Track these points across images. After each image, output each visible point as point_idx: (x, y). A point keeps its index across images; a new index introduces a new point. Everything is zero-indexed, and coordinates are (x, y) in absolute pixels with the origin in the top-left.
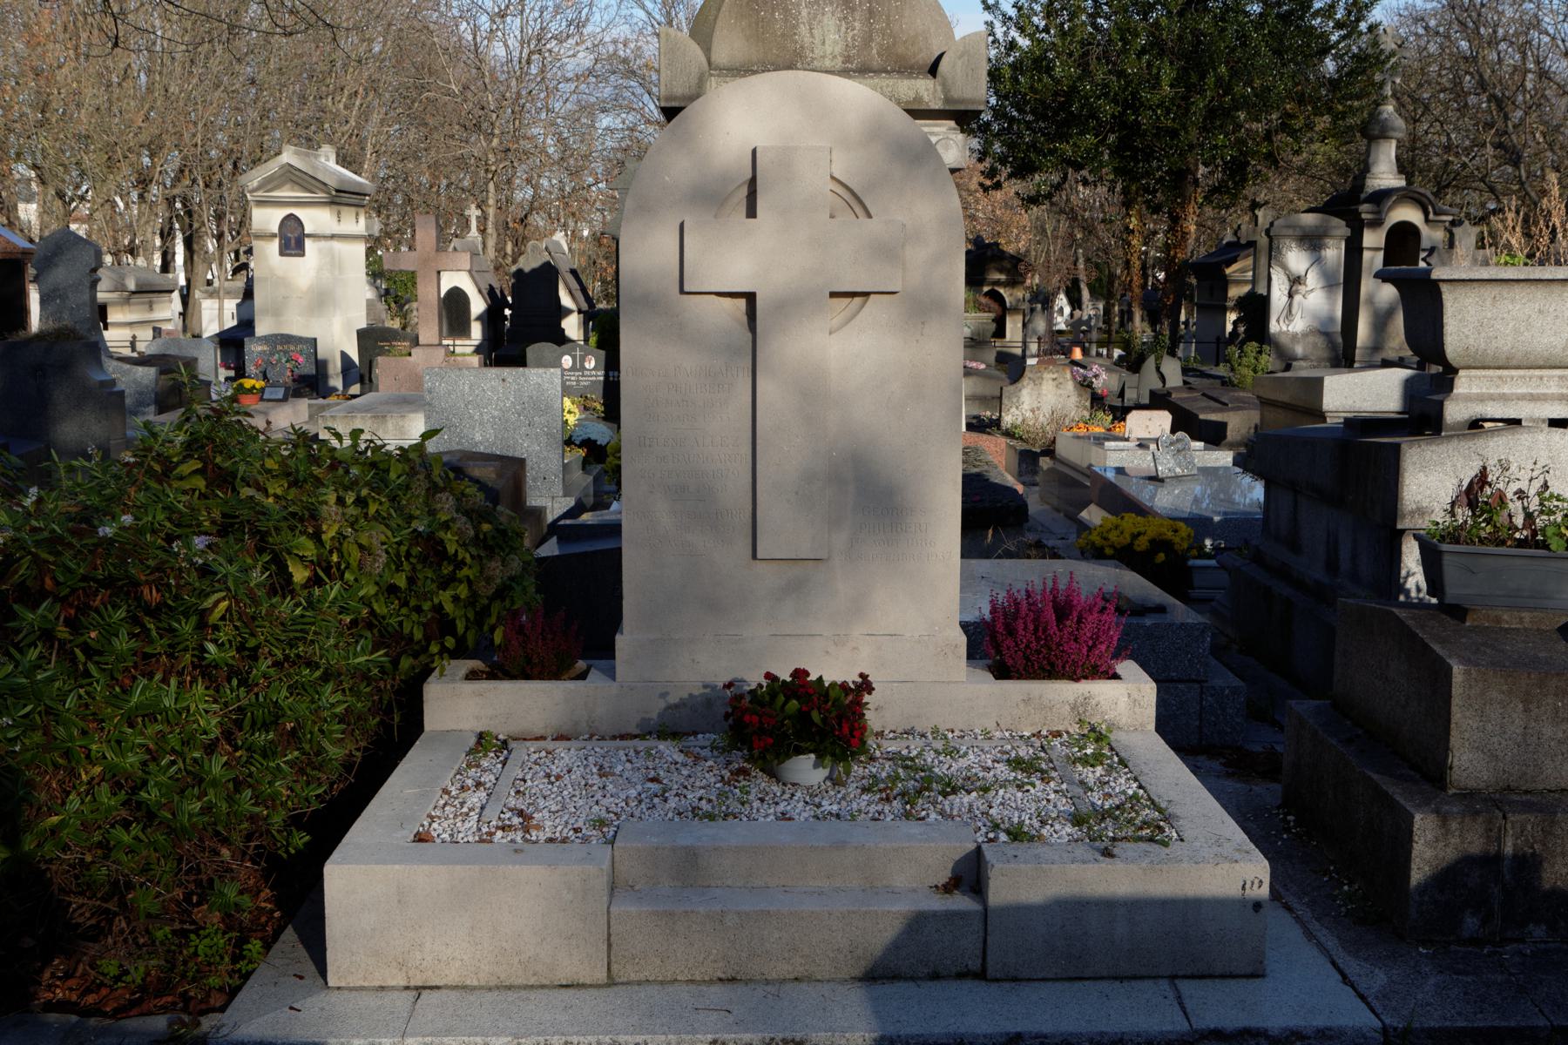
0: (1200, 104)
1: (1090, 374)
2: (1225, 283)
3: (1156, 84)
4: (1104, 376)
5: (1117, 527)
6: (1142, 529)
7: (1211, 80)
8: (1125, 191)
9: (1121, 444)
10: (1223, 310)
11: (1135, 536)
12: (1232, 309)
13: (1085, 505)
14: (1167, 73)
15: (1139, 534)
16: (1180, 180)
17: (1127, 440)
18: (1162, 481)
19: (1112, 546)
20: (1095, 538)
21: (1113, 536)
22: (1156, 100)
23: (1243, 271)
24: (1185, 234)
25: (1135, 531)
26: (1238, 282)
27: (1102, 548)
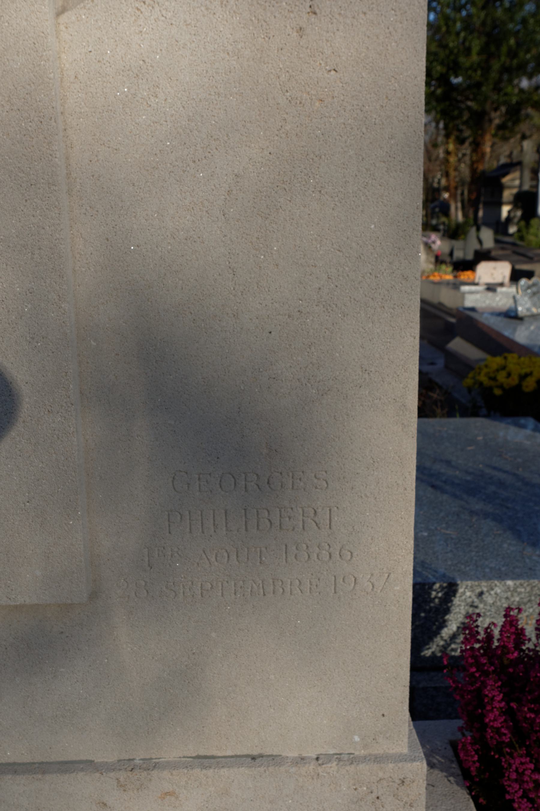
0: (496, 65)
1: (430, 241)
2: (501, 188)
3: (468, 51)
4: (438, 242)
5: (504, 368)
6: (528, 370)
7: (504, 49)
8: (446, 127)
9: (473, 288)
10: (500, 204)
11: (523, 377)
12: (508, 203)
13: (453, 336)
14: (476, 45)
15: (527, 375)
16: (479, 120)
17: (477, 284)
18: (521, 319)
19: (501, 387)
20: (483, 378)
21: (501, 377)
22: (468, 64)
23: (513, 180)
24: (483, 155)
25: (523, 372)
26: (510, 187)
27: (490, 389)
